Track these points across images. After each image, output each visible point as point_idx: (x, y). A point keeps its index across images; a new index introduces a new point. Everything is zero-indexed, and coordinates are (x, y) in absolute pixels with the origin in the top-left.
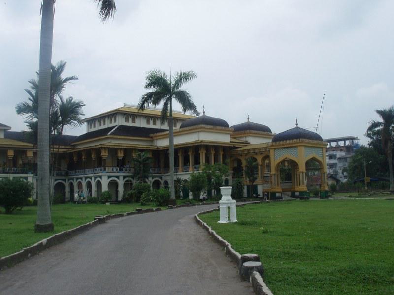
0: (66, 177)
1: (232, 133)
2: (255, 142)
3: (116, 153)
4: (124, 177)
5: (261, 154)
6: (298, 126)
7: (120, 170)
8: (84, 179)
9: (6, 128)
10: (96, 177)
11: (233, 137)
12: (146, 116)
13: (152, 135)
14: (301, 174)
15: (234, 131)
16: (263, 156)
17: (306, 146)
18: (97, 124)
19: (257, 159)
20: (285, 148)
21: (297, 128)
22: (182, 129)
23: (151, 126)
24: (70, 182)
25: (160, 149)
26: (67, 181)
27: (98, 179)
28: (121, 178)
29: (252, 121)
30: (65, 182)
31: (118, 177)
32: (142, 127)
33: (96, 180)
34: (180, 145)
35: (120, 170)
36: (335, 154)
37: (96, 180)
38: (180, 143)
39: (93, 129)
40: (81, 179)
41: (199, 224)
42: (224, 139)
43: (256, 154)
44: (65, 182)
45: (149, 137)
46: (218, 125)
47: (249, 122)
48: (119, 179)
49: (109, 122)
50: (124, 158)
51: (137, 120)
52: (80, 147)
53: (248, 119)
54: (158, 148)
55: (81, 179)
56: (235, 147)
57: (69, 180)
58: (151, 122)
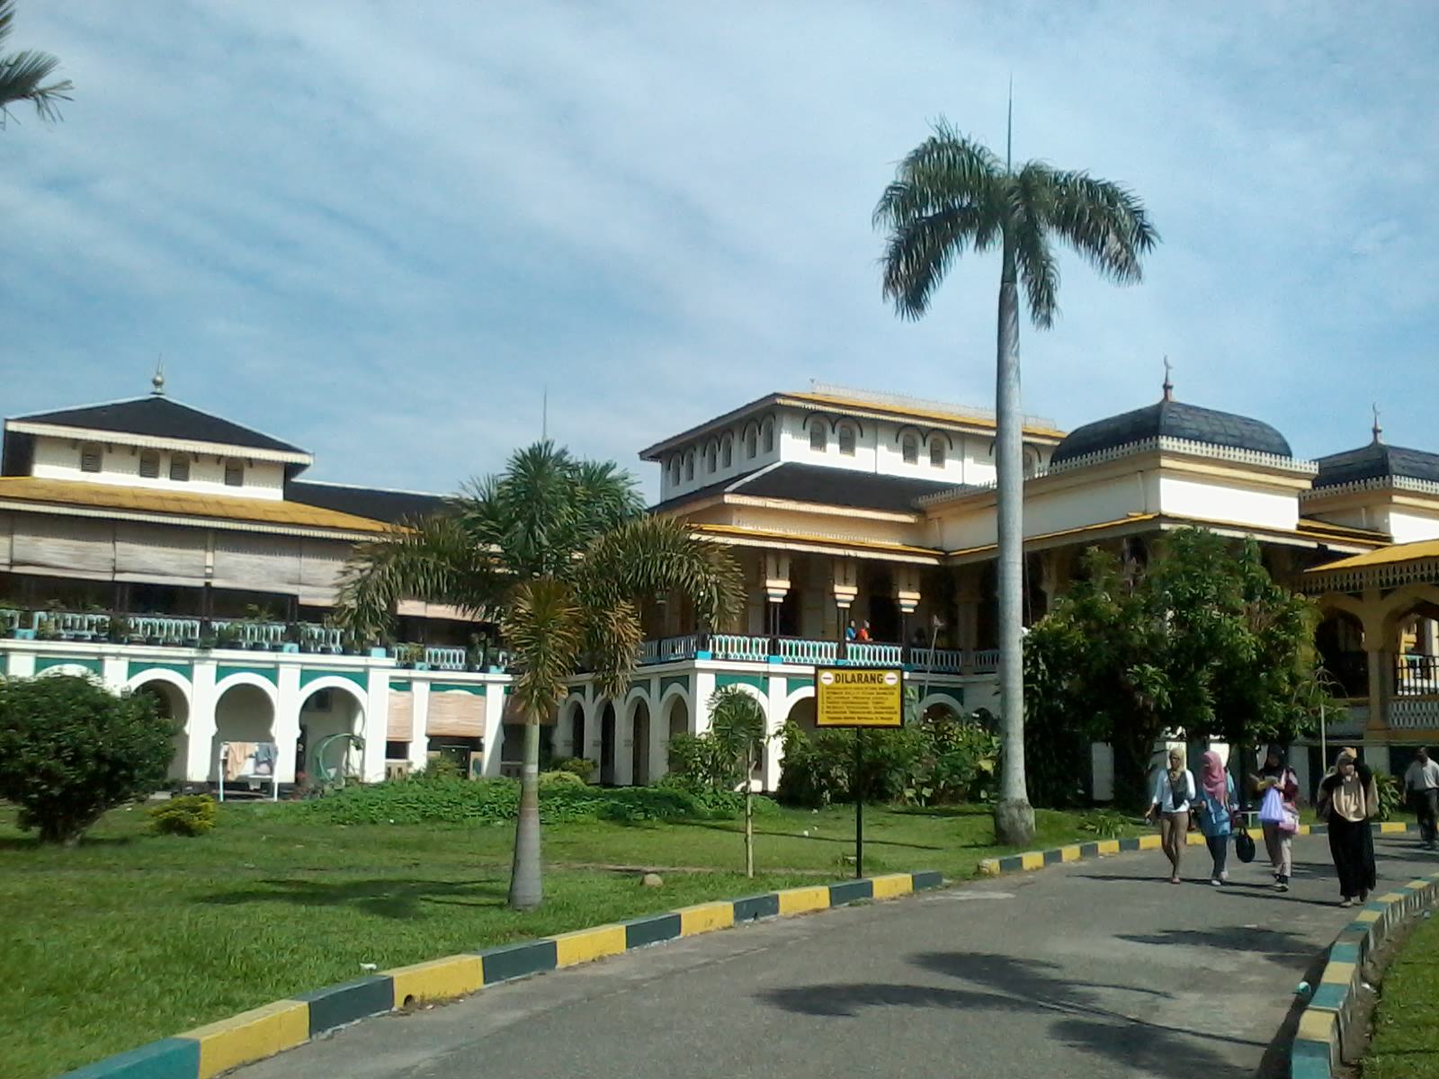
1: (1307, 485)
3: (761, 575)
5: (1385, 593)
7: (774, 649)
10: (665, 682)
15: (1317, 482)
18: (701, 463)
19: (1362, 617)
22: (1059, 466)
24: (600, 697)
25: (959, 562)
28: (778, 685)
29: (173, 396)
32: (881, 471)
33: (630, 698)
35: (774, 649)
36: (117, 679)
37: (630, 698)
39: (686, 488)
40: (646, 684)
41: (1141, 937)
43: (1359, 596)
48: (365, 686)
49: (706, 468)
50: (792, 596)
51: (847, 445)
52: (747, 528)
55: (581, 690)
57: (571, 690)
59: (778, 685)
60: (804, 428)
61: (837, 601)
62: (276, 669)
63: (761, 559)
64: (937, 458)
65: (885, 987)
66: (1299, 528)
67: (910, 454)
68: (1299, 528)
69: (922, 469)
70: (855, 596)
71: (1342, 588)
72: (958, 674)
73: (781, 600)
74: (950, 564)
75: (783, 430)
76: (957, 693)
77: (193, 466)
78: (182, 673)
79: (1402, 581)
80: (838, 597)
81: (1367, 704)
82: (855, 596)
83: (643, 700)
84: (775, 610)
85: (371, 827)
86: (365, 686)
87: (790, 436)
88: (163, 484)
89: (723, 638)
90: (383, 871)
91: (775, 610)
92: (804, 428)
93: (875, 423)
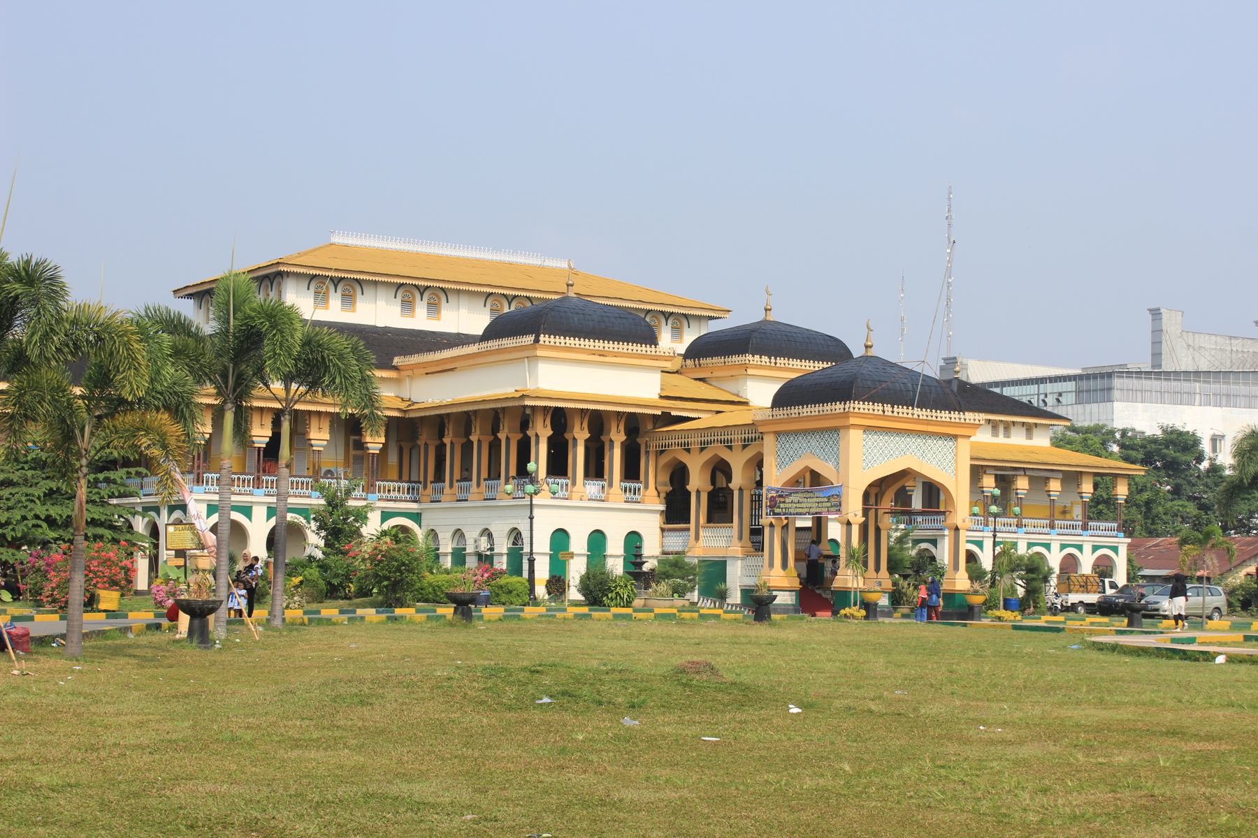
13: (397, 361)
51: (348, 300)
56: (668, 419)
60: (308, 289)
61: (312, 446)
63: (307, 417)
64: (434, 308)
67: (408, 306)
68: (661, 397)
69: (420, 320)
70: (270, 438)
72: (308, 497)
73: (378, 452)
75: (288, 290)
76: (417, 517)
77: (1012, 428)
78: (1077, 549)
81: (688, 529)
82: (270, 438)
84: (373, 458)
86: (1081, 552)
87: (384, 303)
88: (1001, 439)
89: (382, 483)
91: (373, 458)
92: (308, 289)
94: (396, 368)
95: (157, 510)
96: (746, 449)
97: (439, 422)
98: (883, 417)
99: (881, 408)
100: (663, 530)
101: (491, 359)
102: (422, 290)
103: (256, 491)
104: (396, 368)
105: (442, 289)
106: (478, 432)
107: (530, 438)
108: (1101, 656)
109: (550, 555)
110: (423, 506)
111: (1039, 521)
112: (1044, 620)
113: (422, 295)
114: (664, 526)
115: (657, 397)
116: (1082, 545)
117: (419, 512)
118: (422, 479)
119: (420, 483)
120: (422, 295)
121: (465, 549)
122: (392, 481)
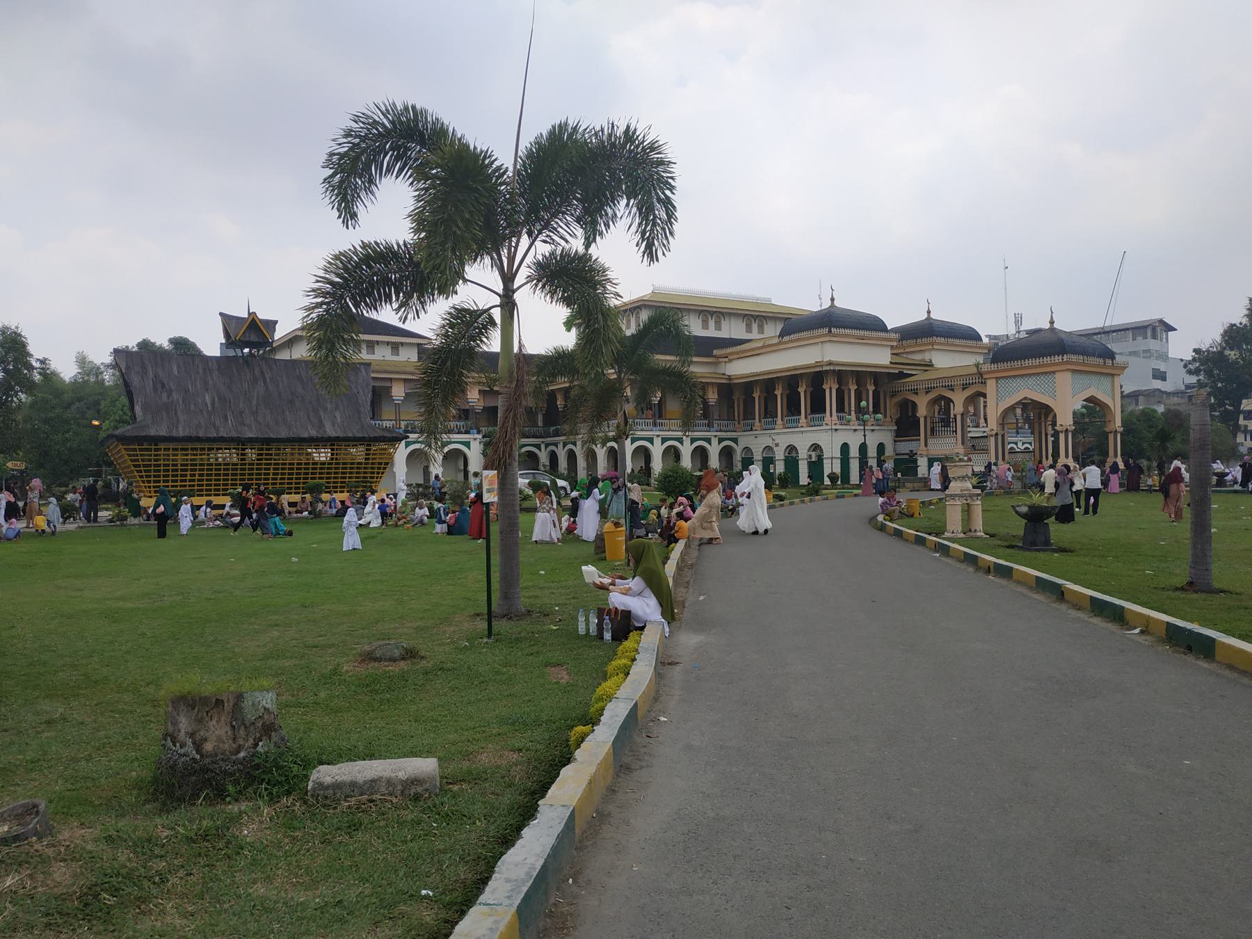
0: (542, 440)
1: (895, 344)
2: (945, 360)
4: (721, 440)
5: (927, 393)
6: (1055, 326)
8: (561, 446)
9: (420, 341)
11: (895, 352)
12: (702, 311)
13: (715, 352)
14: (1111, 437)
16: (968, 393)
17: (1074, 371)
20: (809, 367)
21: (1052, 329)
23: (712, 332)
24: (566, 448)
26: (543, 447)
27: (570, 446)
29: (842, 303)
30: (540, 450)
31: (708, 441)
34: (759, 375)
38: (758, 370)
42: (878, 357)
44: (540, 450)
45: (711, 355)
46: (868, 326)
47: (929, 318)
51: (725, 324)
53: (929, 312)
54: (730, 378)
55: (556, 445)
56: (902, 375)
58: (712, 323)
59: (657, 441)
61: (469, 402)
62: (737, 439)
65: (490, 583)
66: (891, 363)
68: (891, 363)
71: (911, 390)
74: (732, 382)
76: (735, 440)
78: (734, 442)
79: (934, 388)
80: (394, 398)
81: (919, 440)
83: (554, 451)
85: (1014, 505)
90: (650, 534)
93: (730, 315)
94: (715, 356)
95: (556, 445)
96: (965, 391)
97: (748, 386)
98: (1084, 364)
99: (1111, 362)
100: (895, 441)
101: (768, 349)
102: (712, 313)
103: (654, 429)
104: (715, 356)
105: (763, 316)
106: (781, 389)
107: (800, 393)
108: (1017, 516)
109: (841, 458)
110: (739, 434)
111: (388, 422)
112: (97, 525)
113: (755, 321)
114: (896, 439)
115: (889, 363)
116: (737, 439)
117: (468, 440)
118: (736, 419)
119: (734, 420)
120: (755, 321)
121: (753, 458)
122: (724, 420)
